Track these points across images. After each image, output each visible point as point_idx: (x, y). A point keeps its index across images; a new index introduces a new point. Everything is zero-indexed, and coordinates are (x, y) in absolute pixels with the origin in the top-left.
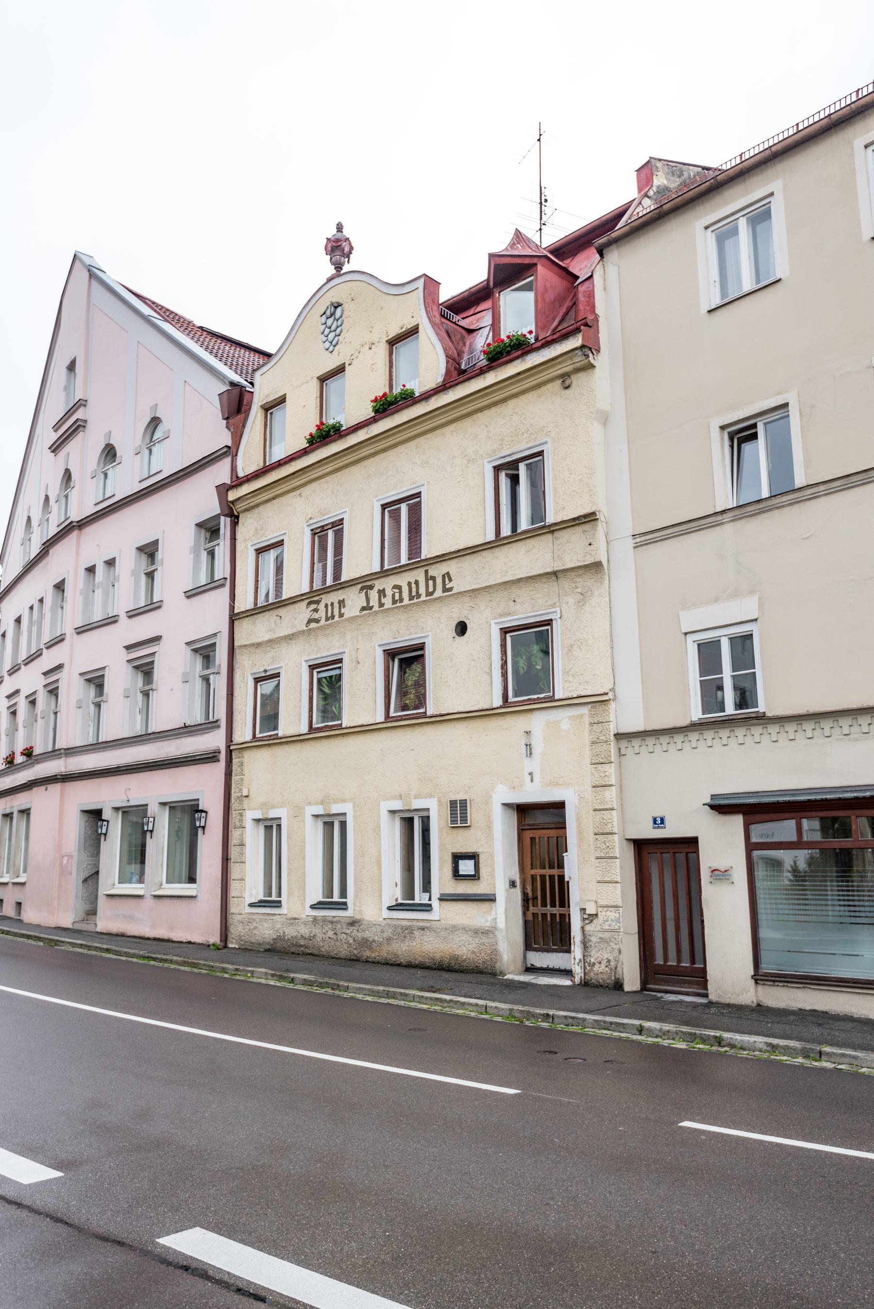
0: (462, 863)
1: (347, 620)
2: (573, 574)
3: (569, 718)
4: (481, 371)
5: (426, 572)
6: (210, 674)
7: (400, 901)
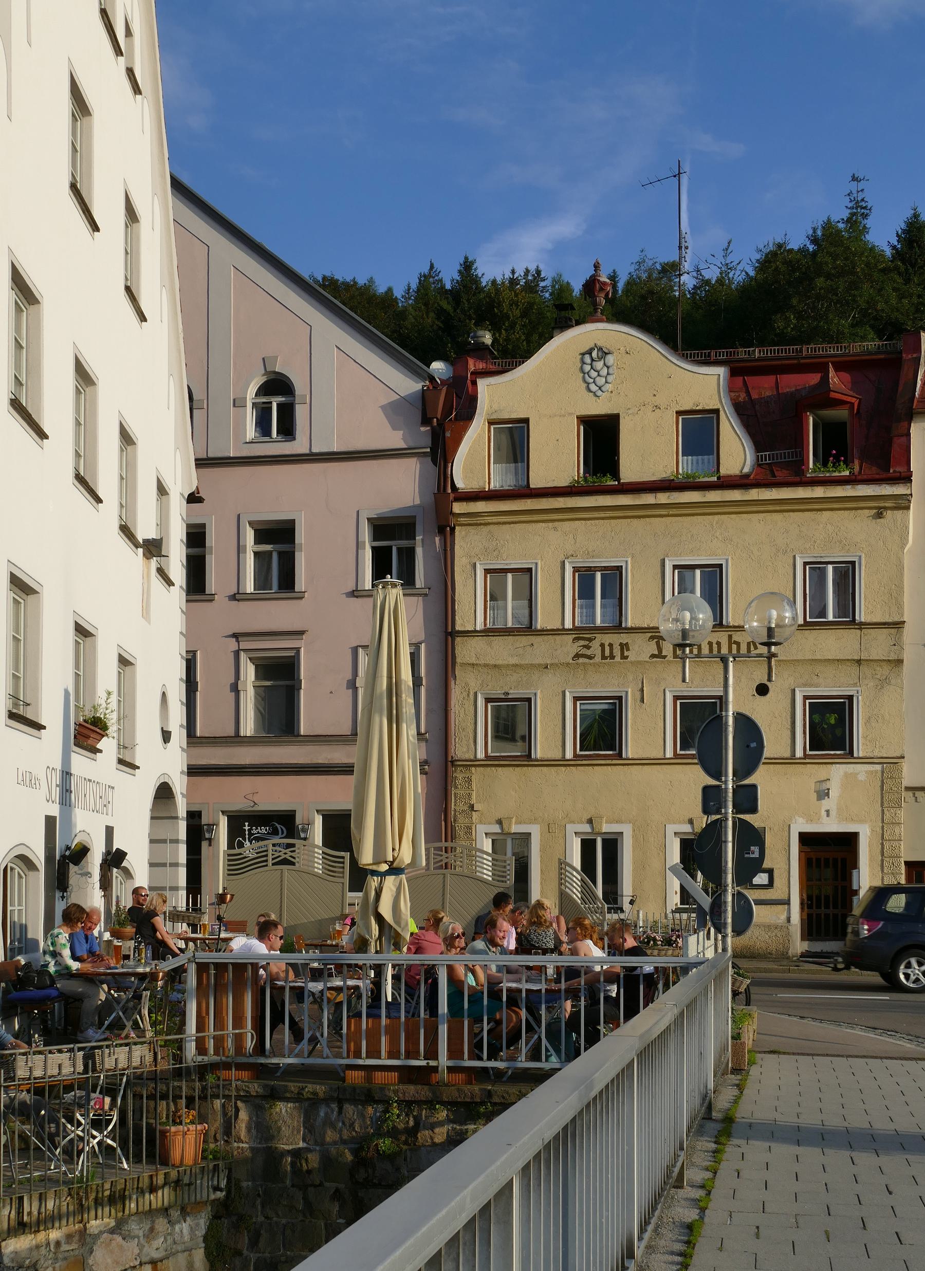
0: (766, 882)
1: (631, 662)
2: (875, 664)
3: (866, 772)
4: (67, 791)
5: (730, 637)
6: (511, 953)
7: (679, 906)
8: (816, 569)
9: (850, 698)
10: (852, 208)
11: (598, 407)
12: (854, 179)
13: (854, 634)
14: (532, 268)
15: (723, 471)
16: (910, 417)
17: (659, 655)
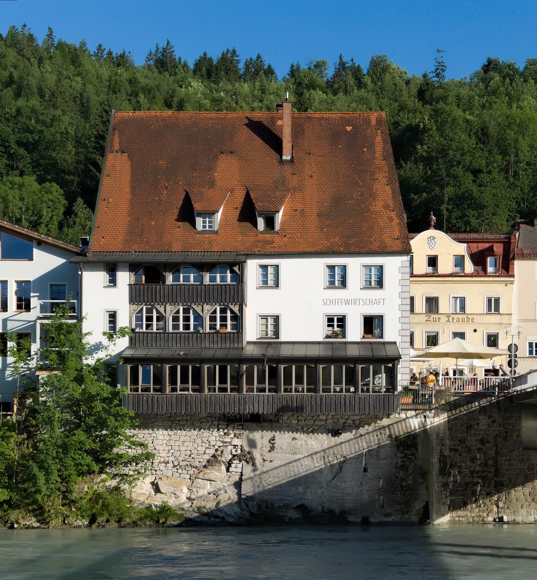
8: (490, 300)
9: (498, 333)
10: (437, 66)
11: (432, 253)
12: (438, 51)
13: (499, 316)
14: (231, 50)
15: (466, 272)
16: (514, 259)
17: (448, 321)
